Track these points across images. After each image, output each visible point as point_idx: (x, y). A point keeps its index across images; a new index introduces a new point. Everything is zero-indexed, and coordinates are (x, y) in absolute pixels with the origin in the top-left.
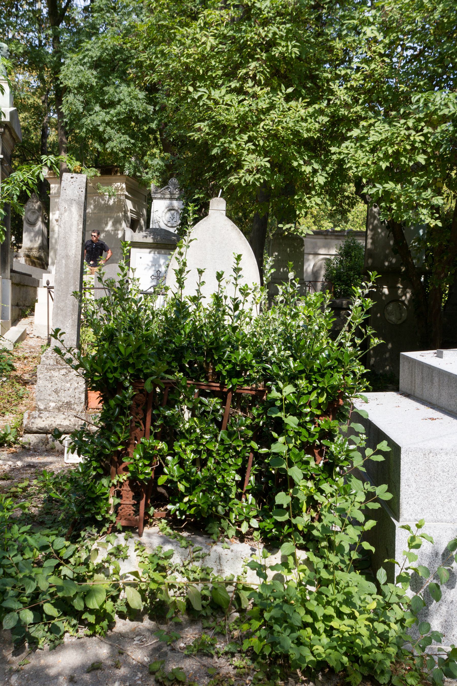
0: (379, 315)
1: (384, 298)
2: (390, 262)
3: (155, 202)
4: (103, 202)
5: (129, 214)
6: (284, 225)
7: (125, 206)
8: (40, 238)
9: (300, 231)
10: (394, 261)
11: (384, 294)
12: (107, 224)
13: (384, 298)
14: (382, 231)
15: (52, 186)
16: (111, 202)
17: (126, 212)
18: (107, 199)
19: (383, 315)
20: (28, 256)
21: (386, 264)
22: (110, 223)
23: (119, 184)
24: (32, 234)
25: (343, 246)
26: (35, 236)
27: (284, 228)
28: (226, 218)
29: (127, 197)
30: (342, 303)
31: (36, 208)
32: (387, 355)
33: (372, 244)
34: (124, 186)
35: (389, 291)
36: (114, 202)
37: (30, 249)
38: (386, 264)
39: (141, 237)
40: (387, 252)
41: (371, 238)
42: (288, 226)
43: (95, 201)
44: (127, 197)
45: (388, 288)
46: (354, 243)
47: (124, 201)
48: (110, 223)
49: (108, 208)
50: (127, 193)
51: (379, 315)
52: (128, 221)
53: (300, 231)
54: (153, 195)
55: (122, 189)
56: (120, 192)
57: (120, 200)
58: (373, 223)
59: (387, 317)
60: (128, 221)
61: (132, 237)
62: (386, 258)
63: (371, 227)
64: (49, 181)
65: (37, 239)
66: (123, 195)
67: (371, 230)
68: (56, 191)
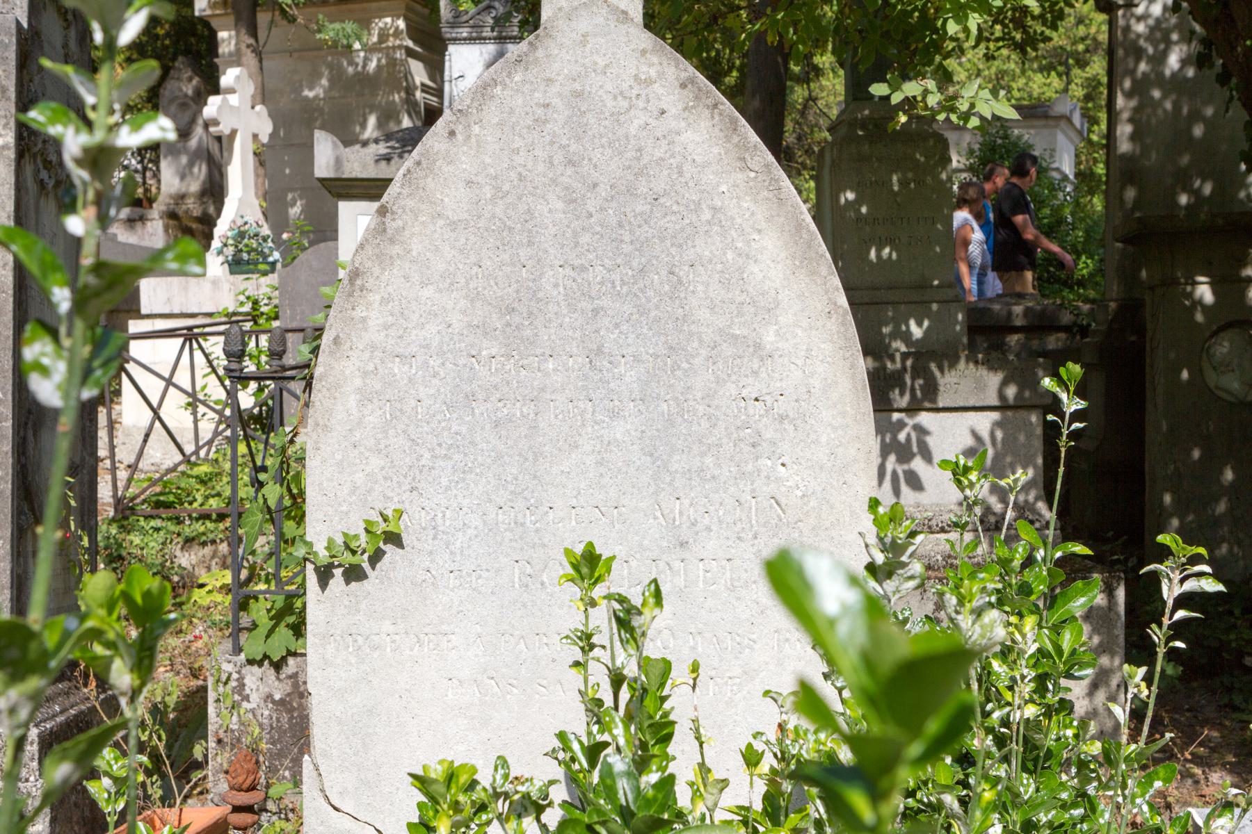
0: (1185, 375)
1: (1199, 317)
2: (1196, 193)
3: (452, 49)
4: (351, 70)
5: (419, 95)
6: (895, 88)
7: (408, 74)
8: (204, 168)
9: (963, 106)
10: (1207, 189)
11: (1200, 302)
12: (363, 125)
13: (1199, 317)
14: (1165, 96)
15: (222, 35)
16: (373, 65)
17: (410, 91)
18: (360, 61)
19: (1197, 373)
20: (172, 215)
21: (1184, 199)
22: (372, 121)
23: (389, 20)
24: (184, 160)
25: (976, 147)
26: (191, 164)
27: (896, 98)
28: (647, 39)
29: (410, 53)
30: (1010, 313)
31: (190, 92)
32: (1222, 507)
33: (1133, 138)
34: (401, 24)
35: (1215, 292)
36: (379, 66)
37: (181, 197)
38: (1184, 199)
39: (370, 160)
40: (1185, 160)
41: (1131, 120)
42: (911, 88)
43: (330, 67)
44: (410, 53)
45: (1212, 284)
46: (1006, 137)
47: (404, 63)
48: (372, 121)
49: (365, 82)
50: (410, 43)
51: (1185, 375)
52: (418, 113)
53: (963, 106)
54: (447, 32)
55: (397, 33)
56: (391, 42)
57: (392, 62)
58: (1132, 72)
59: (1211, 378)
60: (418, 113)
61: (338, 162)
62: (1183, 180)
63: (1127, 84)
64: (214, 23)
65: (196, 170)
66: (400, 47)
67: (1129, 95)
68: (232, 47)
